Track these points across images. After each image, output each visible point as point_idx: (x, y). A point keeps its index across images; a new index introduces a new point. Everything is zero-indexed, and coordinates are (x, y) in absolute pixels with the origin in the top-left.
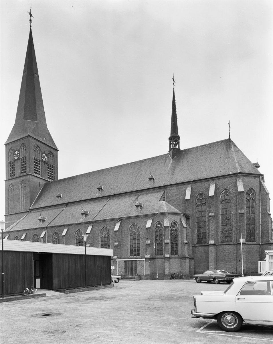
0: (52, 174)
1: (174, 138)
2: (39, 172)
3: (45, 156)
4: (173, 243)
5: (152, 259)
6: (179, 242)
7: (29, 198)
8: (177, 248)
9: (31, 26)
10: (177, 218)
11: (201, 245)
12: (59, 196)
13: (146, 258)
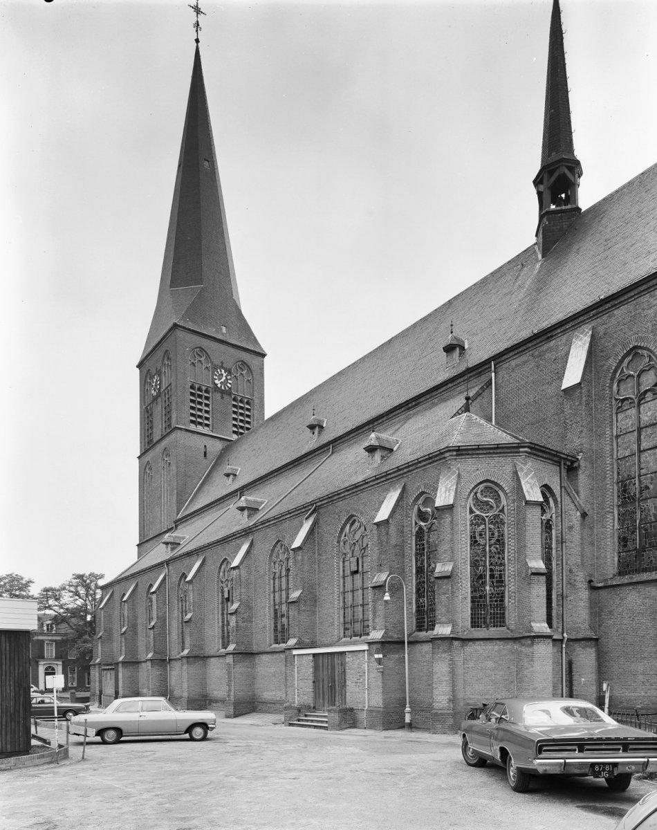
0: (248, 423)
1: (558, 175)
2: (207, 419)
3: (225, 375)
4: (481, 577)
5: (390, 645)
6: (510, 571)
7: (175, 491)
8: (501, 597)
9: (197, 41)
10: (498, 470)
11: (636, 578)
12: (230, 471)
13: (370, 644)
